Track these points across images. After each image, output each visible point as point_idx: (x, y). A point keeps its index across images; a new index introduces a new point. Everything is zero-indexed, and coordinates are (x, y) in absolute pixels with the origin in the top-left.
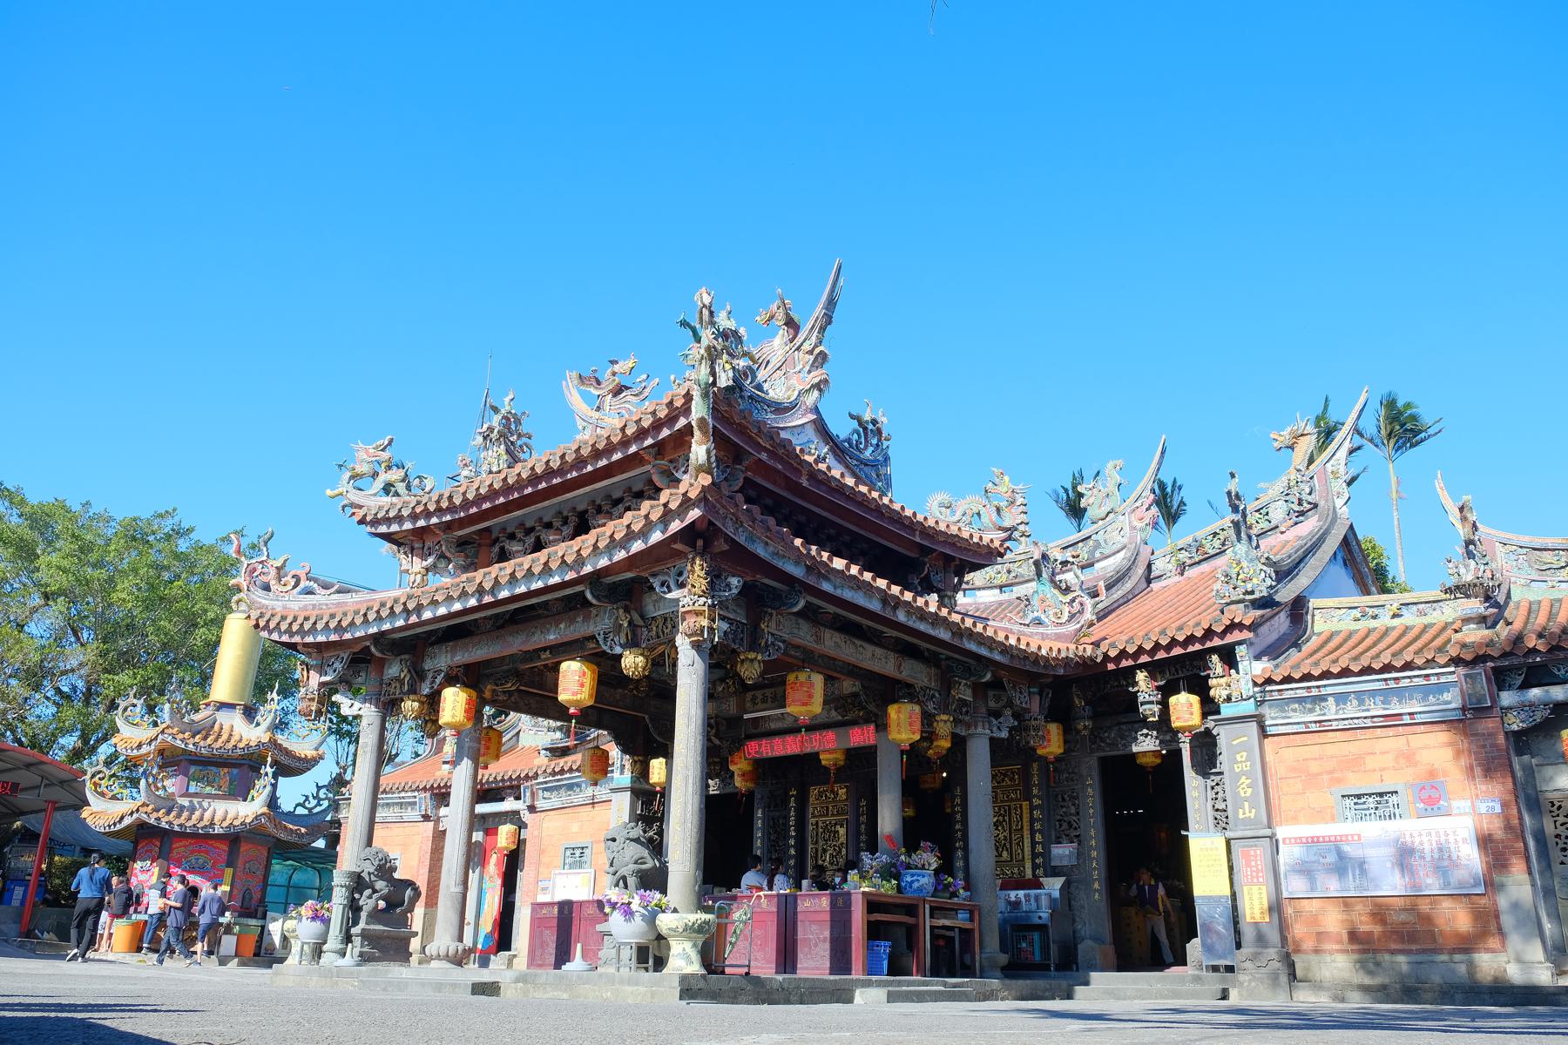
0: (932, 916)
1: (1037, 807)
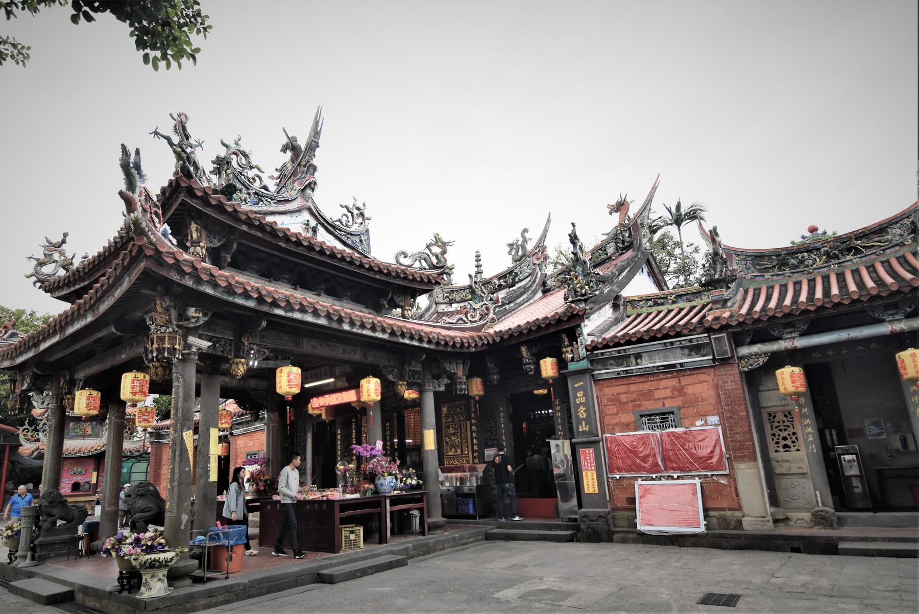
0: (391, 505)
1: (474, 424)
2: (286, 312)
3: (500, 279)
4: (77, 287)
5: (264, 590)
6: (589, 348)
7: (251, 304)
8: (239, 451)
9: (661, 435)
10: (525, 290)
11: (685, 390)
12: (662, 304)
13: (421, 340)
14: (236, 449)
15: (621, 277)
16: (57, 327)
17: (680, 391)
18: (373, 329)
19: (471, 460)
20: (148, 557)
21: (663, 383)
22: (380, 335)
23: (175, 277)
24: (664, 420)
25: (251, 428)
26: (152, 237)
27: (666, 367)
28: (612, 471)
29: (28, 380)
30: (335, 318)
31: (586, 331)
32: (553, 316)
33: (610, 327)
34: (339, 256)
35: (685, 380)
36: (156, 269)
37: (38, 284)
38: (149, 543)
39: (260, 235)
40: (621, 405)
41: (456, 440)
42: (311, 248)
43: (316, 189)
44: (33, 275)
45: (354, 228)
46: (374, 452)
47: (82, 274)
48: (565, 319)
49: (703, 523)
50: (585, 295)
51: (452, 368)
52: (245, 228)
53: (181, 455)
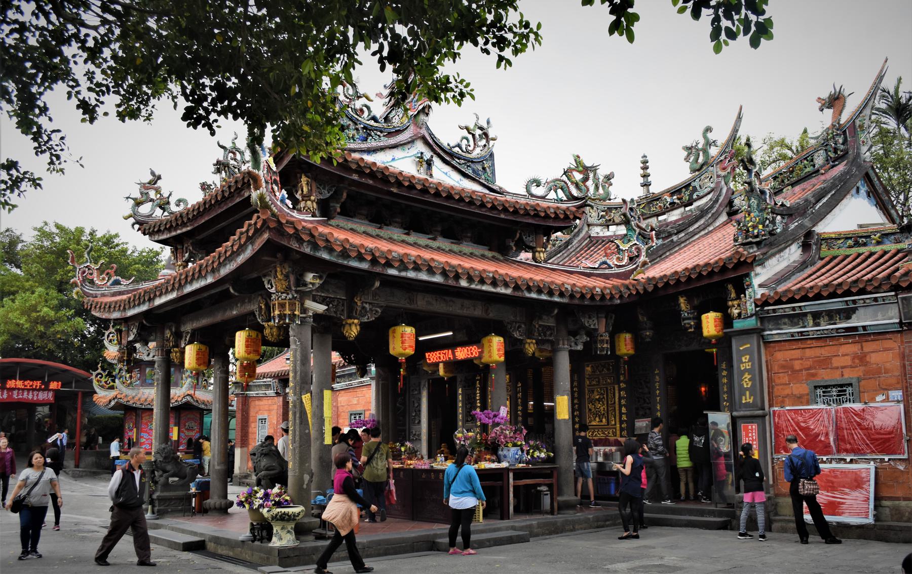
0: (514, 479)
1: (623, 389)
2: (400, 271)
3: (672, 194)
4: (179, 232)
5: (381, 551)
6: (759, 303)
7: (364, 266)
8: (340, 410)
9: (837, 411)
10: (703, 212)
11: (868, 359)
12: (865, 245)
13: (551, 293)
16: (177, 286)
17: (862, 359)
18: (494, 283)
19: (618, 433)
20: (279, 510)
21: (844, 349)
22: (502, 290)
23: (294, 245)
24: (841, 393)
25: (355, 382)
26: (274, 208)
27: (848, 329)
28: (777, 452)
29: (135, 331)
30: (452, 275)
31: (756, 282)
32: (716, 262)
33: (793, 274)
34: (457, 197)
35: (869, 347)
36: (277, 239)
37: (137, 226)
38: (277, 499)
39: (371, 182)
40: (794, 374)
41: (602, 407)
42: (425, 191)
43: (431, 113)
44: (130, 216)
45: (477, 153)
46: (497, 420)
47: (185, 220)
48: (730, 266)
49: (871, 512)
50: (757, 237)
51: (591, 323)
52: (355, 177)
53: (301, 417)
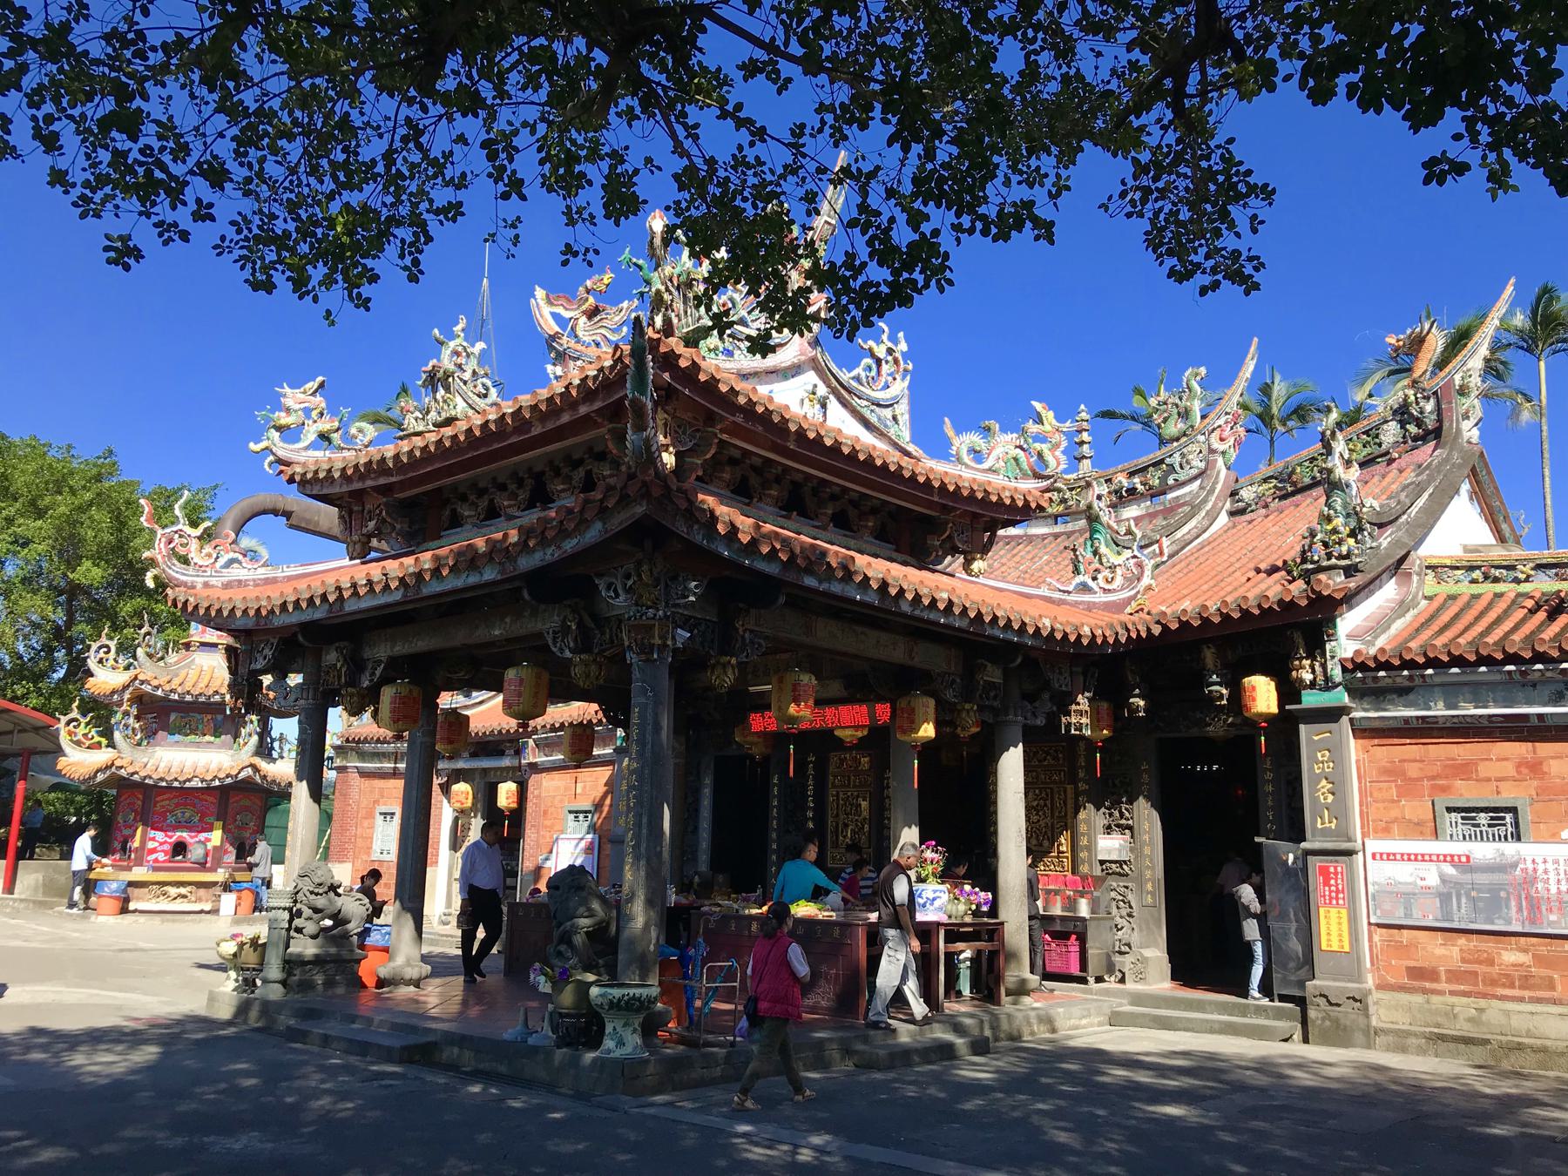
6: (1350, 666)
14: (539, 797)
15: (1414, 510)
29: (269, 653)
35: (1545, 749)
50: (1347, 557)
53: (650, 823)
